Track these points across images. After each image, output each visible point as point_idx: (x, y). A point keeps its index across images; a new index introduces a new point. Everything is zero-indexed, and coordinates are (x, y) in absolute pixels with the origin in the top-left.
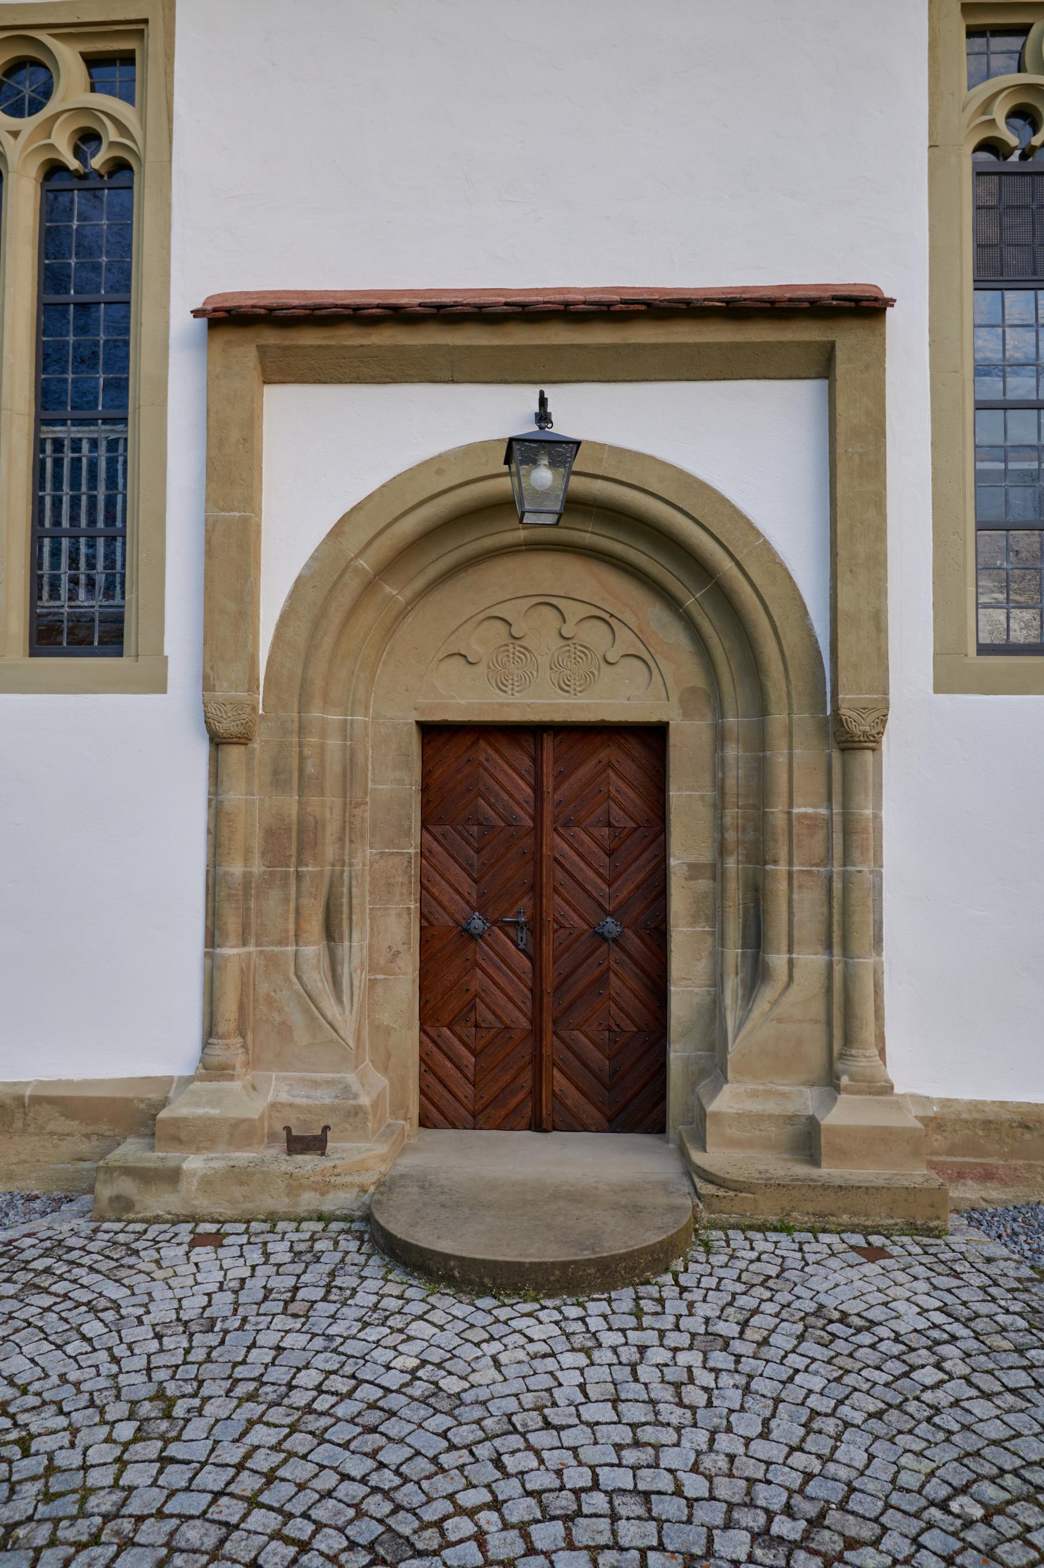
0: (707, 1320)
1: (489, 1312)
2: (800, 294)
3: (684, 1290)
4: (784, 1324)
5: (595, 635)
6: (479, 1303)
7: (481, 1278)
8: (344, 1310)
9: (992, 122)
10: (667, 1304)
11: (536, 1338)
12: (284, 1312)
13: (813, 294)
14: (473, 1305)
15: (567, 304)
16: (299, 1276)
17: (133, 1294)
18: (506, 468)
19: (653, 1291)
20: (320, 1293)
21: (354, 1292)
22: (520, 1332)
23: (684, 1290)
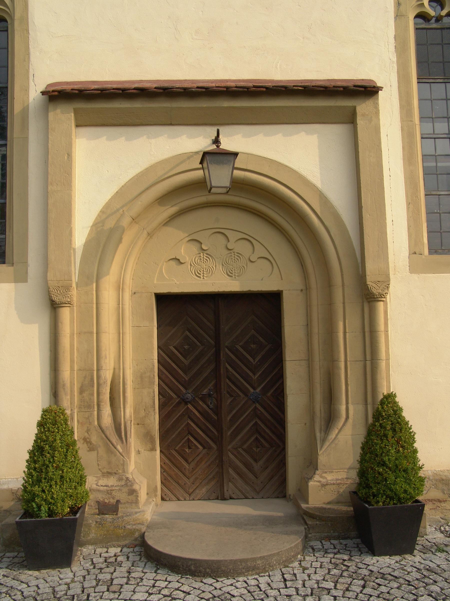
0: (318, 582)
1: (211, 585)
2: (339, 84)
3: (305, 569)
4: (355, 581)
5: (244, 248)
6: (204, 581)
7: (205, 569)
8: (138, 588)
9: (422, 5)
10: (298, 576)
11: (236, 595)
12: (108, 590)
13: (345, 84)
14: (202, 582)
15: (227, 88)
16: (112, 574)
17: (29, 586)
18: (200, 166)
19: (290, 569)
20: (125, 580)
21: (142, 579)
22: (228, 593)
23: (305, 569)
